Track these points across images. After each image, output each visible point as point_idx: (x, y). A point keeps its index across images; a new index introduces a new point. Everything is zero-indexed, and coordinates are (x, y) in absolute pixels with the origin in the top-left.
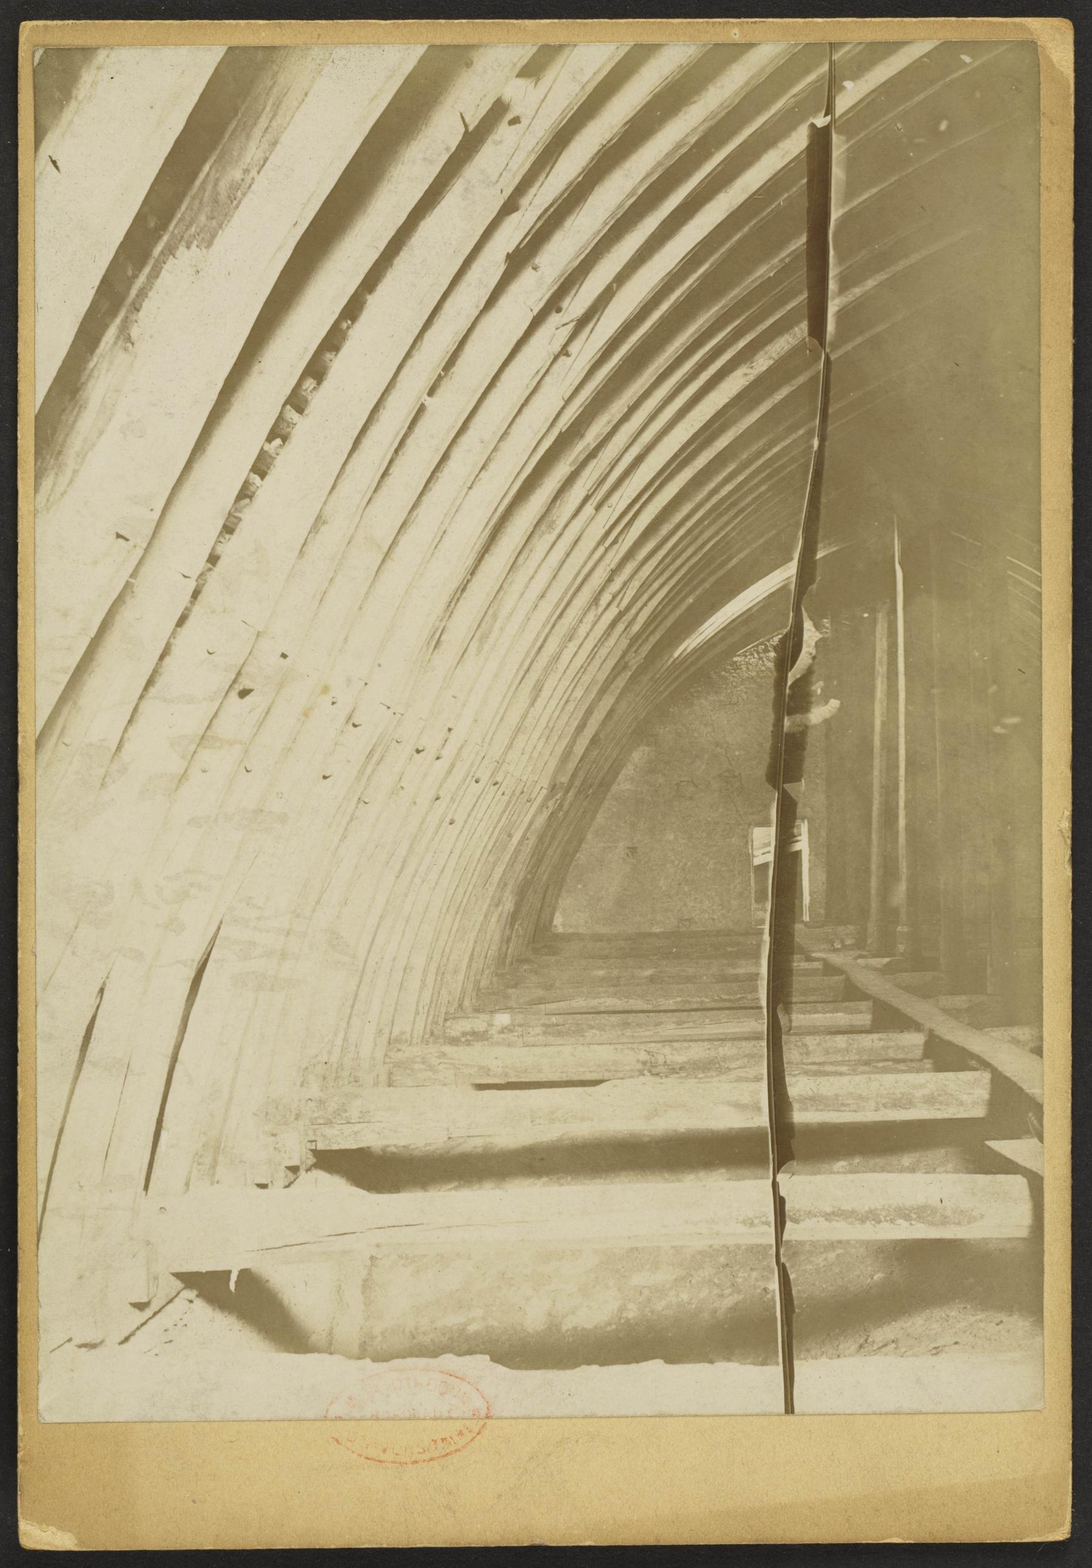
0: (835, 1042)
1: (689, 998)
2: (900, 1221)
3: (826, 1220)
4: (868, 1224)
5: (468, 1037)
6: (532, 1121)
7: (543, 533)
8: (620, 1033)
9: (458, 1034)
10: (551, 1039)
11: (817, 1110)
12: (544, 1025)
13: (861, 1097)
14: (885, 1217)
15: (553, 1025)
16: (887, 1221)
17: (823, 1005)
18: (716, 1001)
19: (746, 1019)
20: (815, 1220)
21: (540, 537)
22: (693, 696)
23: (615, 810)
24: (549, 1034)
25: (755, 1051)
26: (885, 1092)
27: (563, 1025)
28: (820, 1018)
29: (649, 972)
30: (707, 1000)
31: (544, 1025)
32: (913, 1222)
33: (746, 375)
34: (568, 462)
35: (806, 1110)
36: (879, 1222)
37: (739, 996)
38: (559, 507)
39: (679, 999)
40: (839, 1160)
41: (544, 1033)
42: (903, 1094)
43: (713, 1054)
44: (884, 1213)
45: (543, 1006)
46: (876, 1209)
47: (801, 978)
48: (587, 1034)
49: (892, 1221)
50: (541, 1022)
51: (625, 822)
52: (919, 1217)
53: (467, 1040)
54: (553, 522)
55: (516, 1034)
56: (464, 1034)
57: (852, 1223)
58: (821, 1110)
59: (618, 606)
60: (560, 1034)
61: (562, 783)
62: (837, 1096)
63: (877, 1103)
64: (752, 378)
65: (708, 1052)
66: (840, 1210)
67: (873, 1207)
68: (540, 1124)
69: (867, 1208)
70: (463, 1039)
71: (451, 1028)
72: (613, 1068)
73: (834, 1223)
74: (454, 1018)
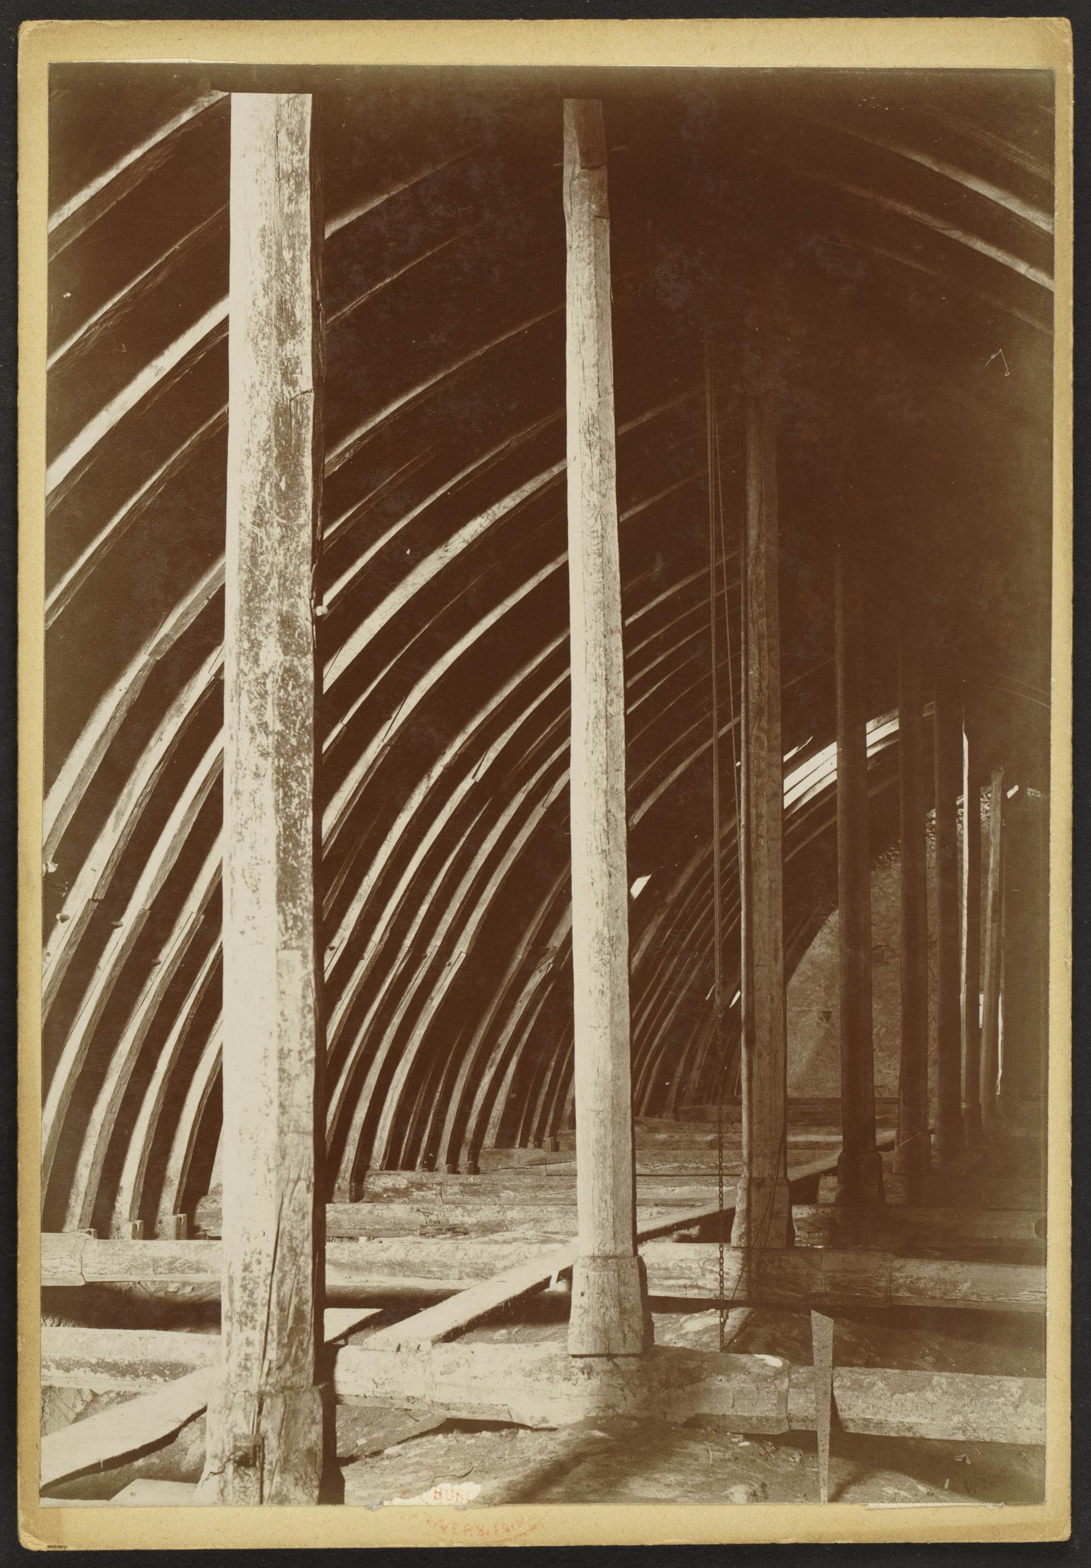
0: (392, 1210)
1: (685, 1164)
2: (155, 1377)
3: (92, 1370)
4: (128, 1378)
5: (390, 1193)
6: (154, 1271)
7: (172, 716)
8: (533, 1194)
9: (381, 1190)
10: (467, 1197)
11: (405, 1276)
12: (461, 1184)
13: (445, 1265)
14: (143, 1372)
15: (471, 1185)
16: (144, 1376)
17: (729, 1178)
18: (712, 1168)
19: (655, 1186)
20: (82, 1370)
21: (170, 720)
22: (891, 860)
23: (810, 973)
24: (466, 1193)
25: (541, 1215)
26: (468, 1261)
27: (480, 1185)
28: (662, 1191)
29: (710, 1137)
30: (703, 1167)
31: (461, 1184)
32: (167, 1379)
33: (441, 558)
34: (149, 652)
35: (394, 1275)
36: (138, 1376)
37: (734, 1163)
38: (187, 692)
39: (676, 1165)
40: (500, 1329)
41: (462, 1192)
42: (485, 1264)
43: (500, 1217)
44: (141, 1368)
45: (542, 1167)
46: (135, 1363)
47: (794, 1152)
48: (502, 1195)
49: (149, 1376)
50: (459, 1181)
51: (820, 986)
52: (171, 1373)
53: (388, 1196)
54: (182, 706)
55: (434, 1192)
56: (386, 1190)
57: (114, 1375)
58: (408, 1276)
59: (473, 777)
60: (475, 1193)
61: (555, 948)
62: (423, 1262)
63: (461, 1272)
64: (447, 561)
65: (496, 1215)
66: (103, 1361)
67: (132, 1362)
68: (161, 1273)
69: (126, 1362)
70: (385, 1196)
71: (374, 1183)
72: (407, 1226)
73: (99, 1375)
74: (377, 1175)
